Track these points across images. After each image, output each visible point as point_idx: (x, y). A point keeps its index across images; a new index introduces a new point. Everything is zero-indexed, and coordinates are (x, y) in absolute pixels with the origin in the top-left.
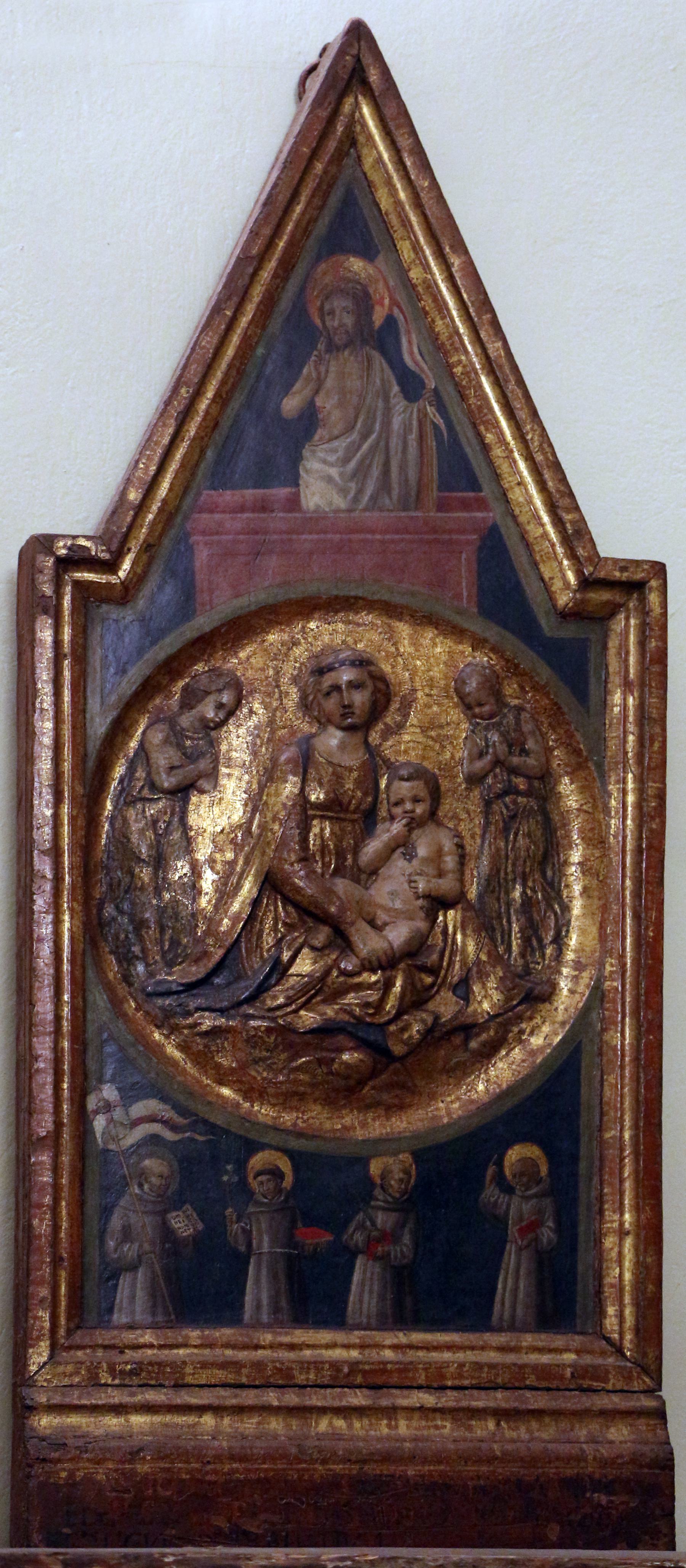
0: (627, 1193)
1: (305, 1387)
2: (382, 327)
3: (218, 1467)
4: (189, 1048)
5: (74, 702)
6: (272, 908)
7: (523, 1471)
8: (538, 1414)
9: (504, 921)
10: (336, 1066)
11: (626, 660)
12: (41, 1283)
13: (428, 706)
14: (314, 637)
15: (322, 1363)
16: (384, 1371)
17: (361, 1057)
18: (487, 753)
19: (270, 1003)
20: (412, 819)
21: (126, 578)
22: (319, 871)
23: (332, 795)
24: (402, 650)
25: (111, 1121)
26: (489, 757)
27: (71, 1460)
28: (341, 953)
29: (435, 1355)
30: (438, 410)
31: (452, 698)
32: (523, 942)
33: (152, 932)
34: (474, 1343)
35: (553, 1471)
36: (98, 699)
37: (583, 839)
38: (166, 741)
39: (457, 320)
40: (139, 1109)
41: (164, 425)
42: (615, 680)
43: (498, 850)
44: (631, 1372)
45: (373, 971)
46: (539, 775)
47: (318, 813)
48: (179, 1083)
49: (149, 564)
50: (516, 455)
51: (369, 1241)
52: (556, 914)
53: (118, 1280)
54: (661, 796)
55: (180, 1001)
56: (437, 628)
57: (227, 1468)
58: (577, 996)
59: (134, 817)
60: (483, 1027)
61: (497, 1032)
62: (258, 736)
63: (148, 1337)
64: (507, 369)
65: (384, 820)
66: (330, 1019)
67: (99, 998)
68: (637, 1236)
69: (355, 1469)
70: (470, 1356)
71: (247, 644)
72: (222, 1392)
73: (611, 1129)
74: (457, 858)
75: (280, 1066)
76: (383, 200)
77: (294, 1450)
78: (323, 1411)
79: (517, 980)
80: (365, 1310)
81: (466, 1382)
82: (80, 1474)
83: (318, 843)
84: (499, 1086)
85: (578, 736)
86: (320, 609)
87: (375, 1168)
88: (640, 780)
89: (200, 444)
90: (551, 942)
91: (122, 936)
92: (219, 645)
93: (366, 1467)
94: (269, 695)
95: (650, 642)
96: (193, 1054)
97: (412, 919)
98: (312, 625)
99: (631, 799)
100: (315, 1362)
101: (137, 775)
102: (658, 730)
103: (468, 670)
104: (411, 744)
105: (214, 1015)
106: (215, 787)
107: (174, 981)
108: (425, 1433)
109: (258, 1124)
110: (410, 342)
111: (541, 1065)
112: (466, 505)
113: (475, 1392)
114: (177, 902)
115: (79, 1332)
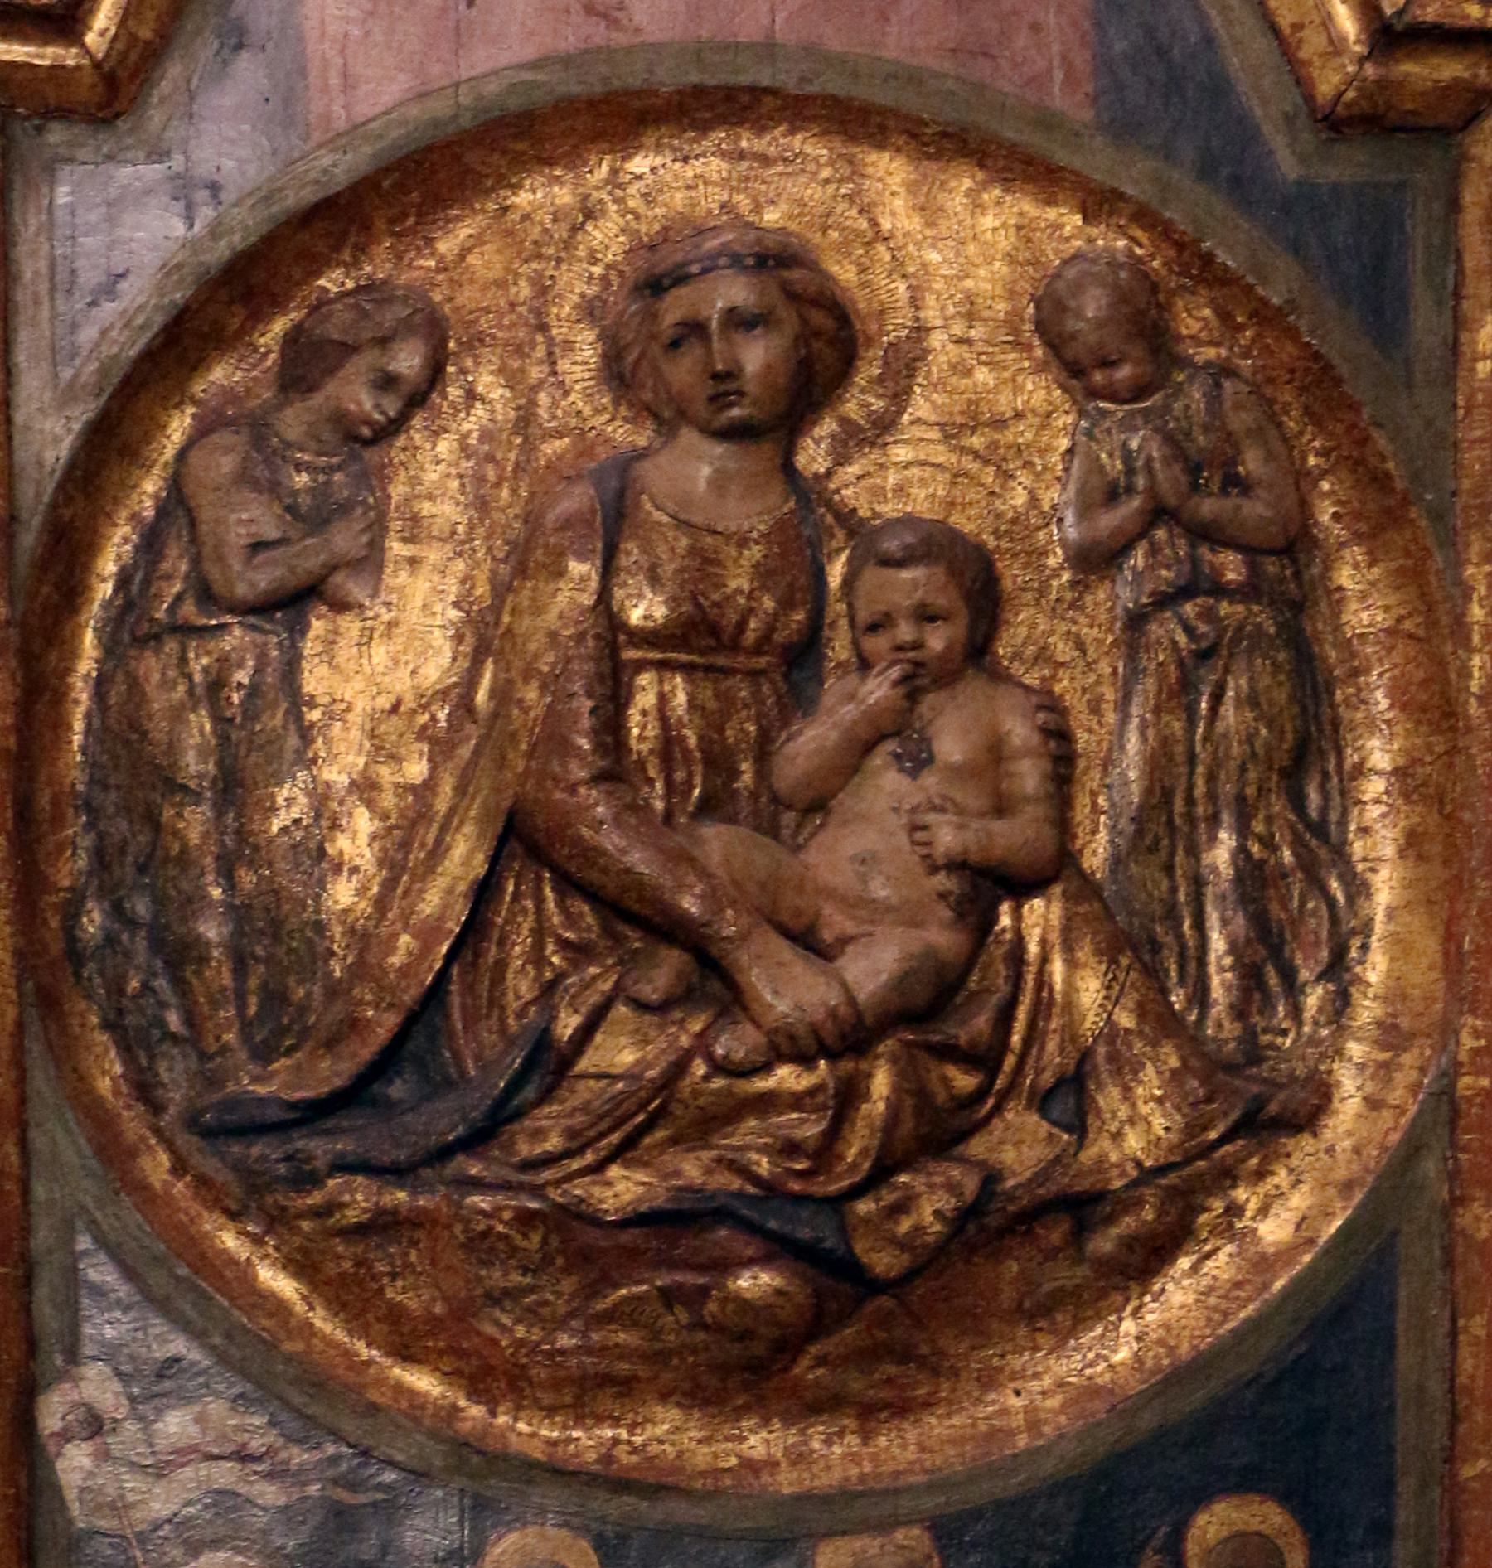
6: (529, 904)
10: (712, 1307)
17: (778, 1282)
19: (526, 1149)
20: (918, 664)
21: (108, 55)
22: (659, 805)
23: (686, 608)
24: (886, 224)
26: (1136, 502)
28: (720, 1015)
31: (1029, 348)
32: (1242, 977)
37: (1404, 707)
38: (244, 478)
45: (805, 1061)
46: (1281, 542)
48: (289, 1359)
52: (1331, 902)
58: (1386, 1114)
59: (156, 677)
60: (1126, 1202)
61: (1161, 1213)
62: (490, 458)
66: (689, 1189)
71: (458, 219)
73: (1477, 1455)
74: (1048, 766)
75: (562, 1310)
83: (651, 732)
84: (1172, 1350)
85: (1381, 441)
90: (1320, 978)
92: (380, 224)
97: (916, 924)
98: (639, 164)
103: (1071, 273)
104: (915, 471)
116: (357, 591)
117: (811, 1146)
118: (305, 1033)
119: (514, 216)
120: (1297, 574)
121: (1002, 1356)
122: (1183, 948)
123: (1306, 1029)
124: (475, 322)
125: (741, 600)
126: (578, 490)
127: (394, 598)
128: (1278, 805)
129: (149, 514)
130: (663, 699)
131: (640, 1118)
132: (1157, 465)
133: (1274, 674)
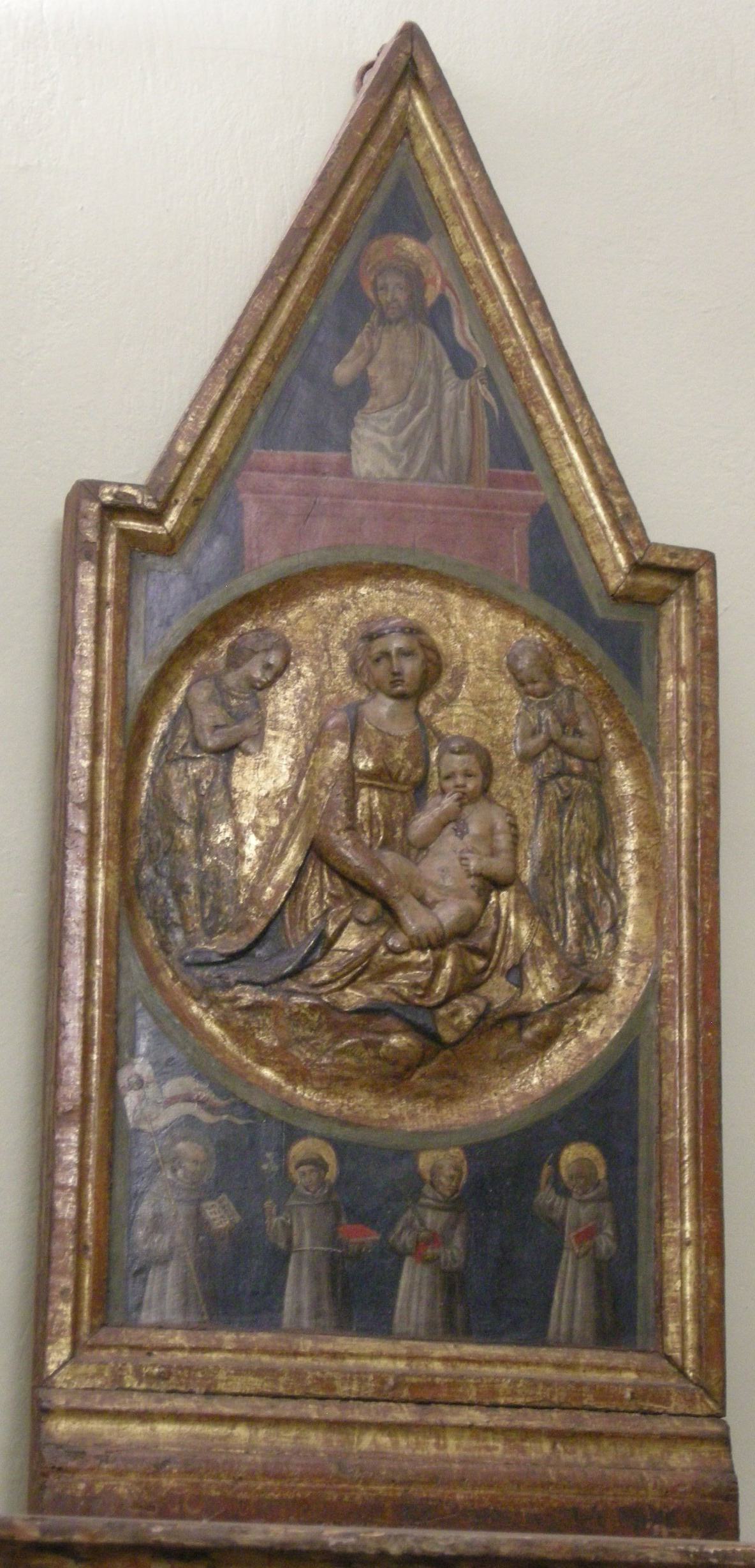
0: (687, 1200)
1: (347, 1399)
2: (434, 306)
3: (252, 1484)
4: (228, 1023)
5: (115, 653)
6: (317, 878)
7: (579, 1499)
8: (597, 1436)
9: (559, 906)
10: (383, 1050)
11: (678, 647)
12: (62, 1273)
13: (479, 680)
14: (365, 603)
15: (366, 1373)
16: (433, 1385)
17: (409, 1041)
18: (540, 732)
19: (314, 979)
20: (464, 794)
21: (173, 530)
22: (367, 842)
23: (381, 764)
24: (454, 622)
25: (141, 1099)
26: (542, 736)
27: (91, 1469)
29: (487, 1370)
30: (490, 389)
33: (192, 896)
34: (530, 1358)
35: (611, 1499)
36: (141, 650)
38: (211, 699)
39: (507, 304)
40: (172, 1087)
41: (215, 381)
42: (667, 666)
43: (552, 832)
44: (694, 1394)
45: (422, 949)
46: (594, 757)
47: (368, 782)
48: (218, 1060)
49: (197, 517)
50: (566, 437)
51: (417, 1242)
52: (612, 903)
53: (147, 1273)
54: (715, 785)
55: (220, 972)
56: (488, 601)
57: (260, 1486)
58: (635, 988)
59: (175, 775)
60: (538, 1016)
61: (551, 1023)
62: (306, 699)
63: (178, 1339)
64: (556, 353)
65: (435, 793)
67: (133, 965)
68: (698, 1247)
69: (399, 1491)
70: (525, 1371)
71: (295, 606)
72: (258, 1402)
75: (325, 1047)
76: (435, 186)
77: (333, 1469)
78: (366, 1426)
79: (573, 969)
80: (413, 1319)
81: (520, 1401)
82: (99, 1487)
84: (555, 1080)
85: (632, 720)
86: (371, 575)
87: (425, 1162)
88: (694, 767)
89: (251, 404)
90: (608, 931)
91: (161, 901)
92: (267, 604)
93: (412, 1489)
94: (318, 658)
95: (701, 630)
96: (233, 1030)
98: (363, 591)
99: (685, 786)
100: (358, 1373)
101: (181, 732)
102: (710, 718)
103: (520, 646)
104: (463, 718)
105: (254, 989)
106: (260, 750)
107: (213, 951)
108: (476, 1454)
109: (301, 1109)
110: (462, 323)
111: (598, 1060)
112: (518, 483)
113: (530, 1411)
114: (219, 867)
115: (104, 1330)
116: (251, 747)
117: (424, 986)
118: (227, 926)
119: (315, 606)
120: (599, 770)
121: (490, 1078)
122: (558, 917)
123: (603, 952)
124: (301, 646)
125: (400, 763)
126: (340, 714)
127: (268, 751)
128: (592, 861)
129: (175, 711)
130: (371, 799)
131: (359, 969)
132: (550, 723)
133: (591, 808)
